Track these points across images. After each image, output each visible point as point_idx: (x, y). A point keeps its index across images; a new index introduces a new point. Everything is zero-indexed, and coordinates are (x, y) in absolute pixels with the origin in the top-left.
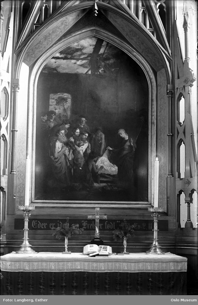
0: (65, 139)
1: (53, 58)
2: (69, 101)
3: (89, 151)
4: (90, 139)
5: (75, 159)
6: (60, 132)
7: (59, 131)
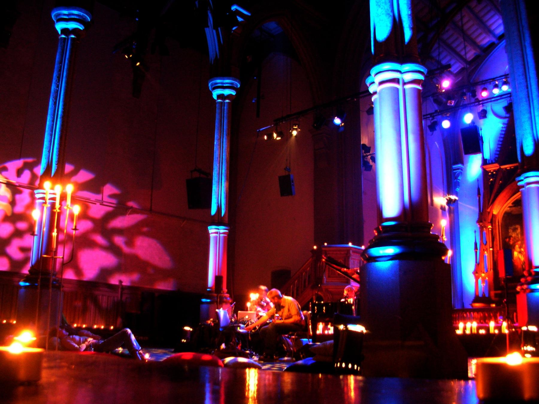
0: (518, 250)
7: (515, 246)
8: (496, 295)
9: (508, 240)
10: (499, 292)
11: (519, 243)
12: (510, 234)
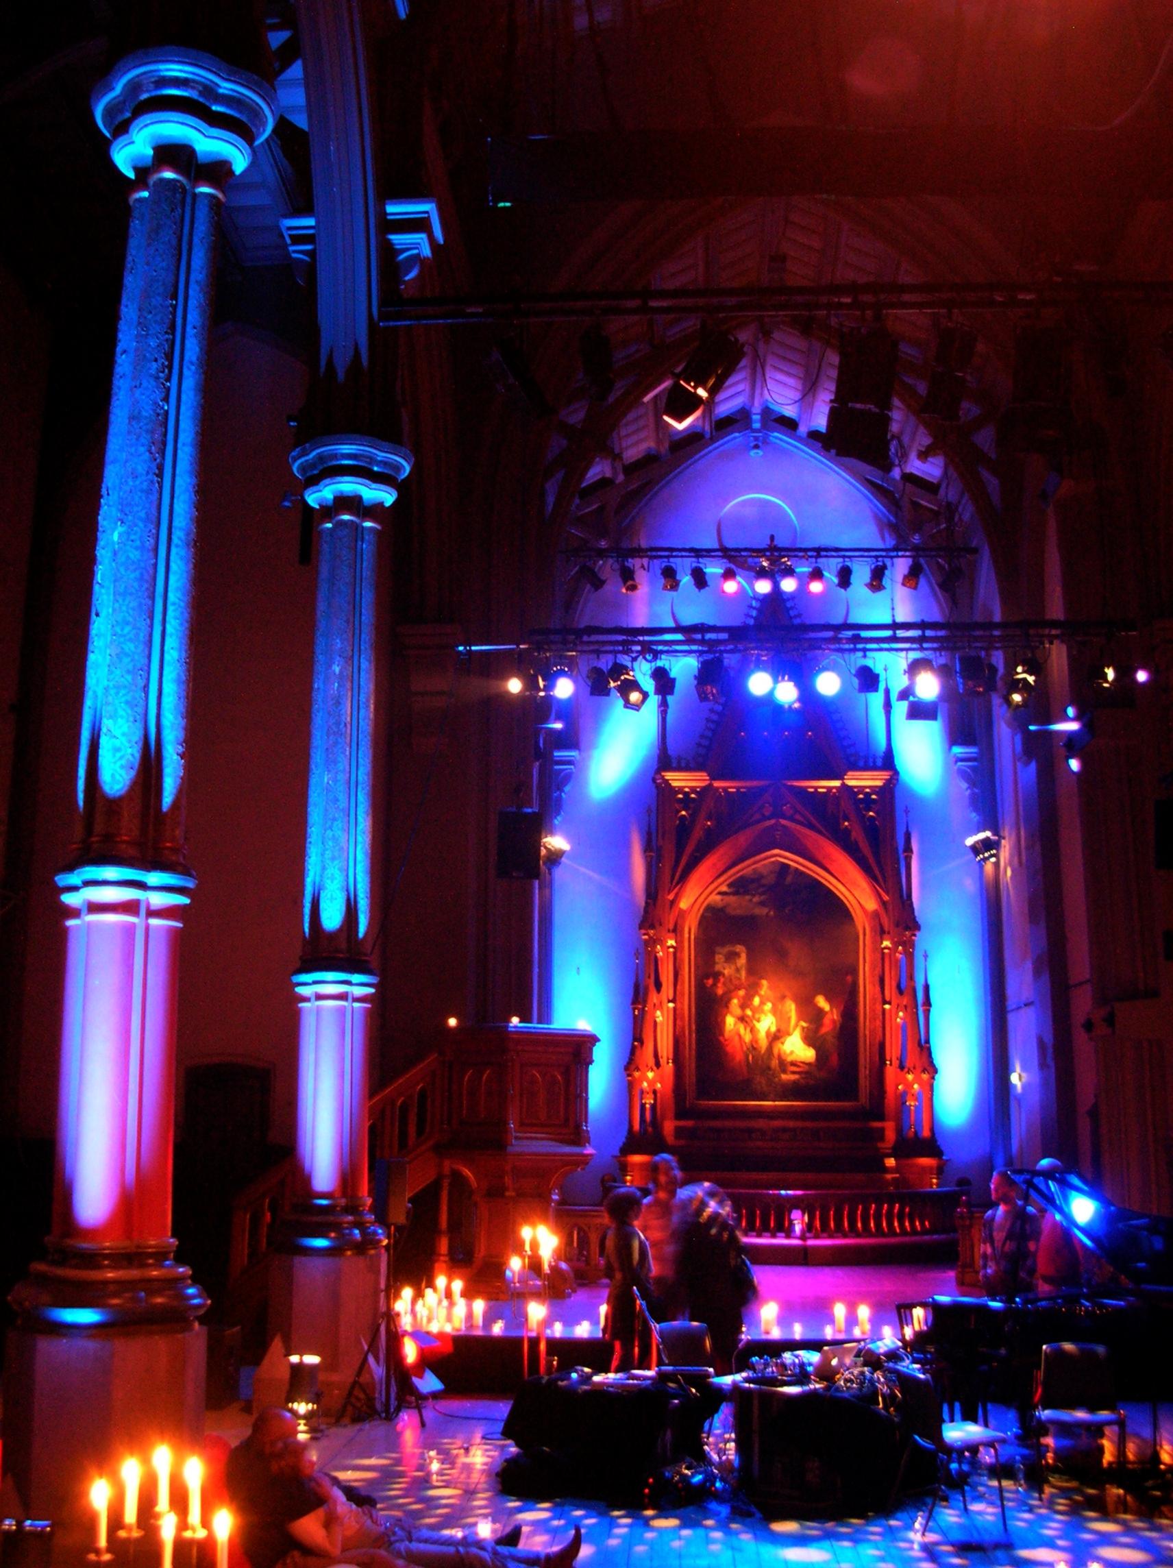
0: (738, 1012)
1: (719, 893)
2: (744, 956)
3: (773, 1029)
4: (774, 1011)
5: (755, 1040)
6: (848, 1388)
7: (729, 1001)
8: (679, 1132)
9: (710, 981)
10: (689, 1123)
11: (742, 993)
12: (718, 967)
